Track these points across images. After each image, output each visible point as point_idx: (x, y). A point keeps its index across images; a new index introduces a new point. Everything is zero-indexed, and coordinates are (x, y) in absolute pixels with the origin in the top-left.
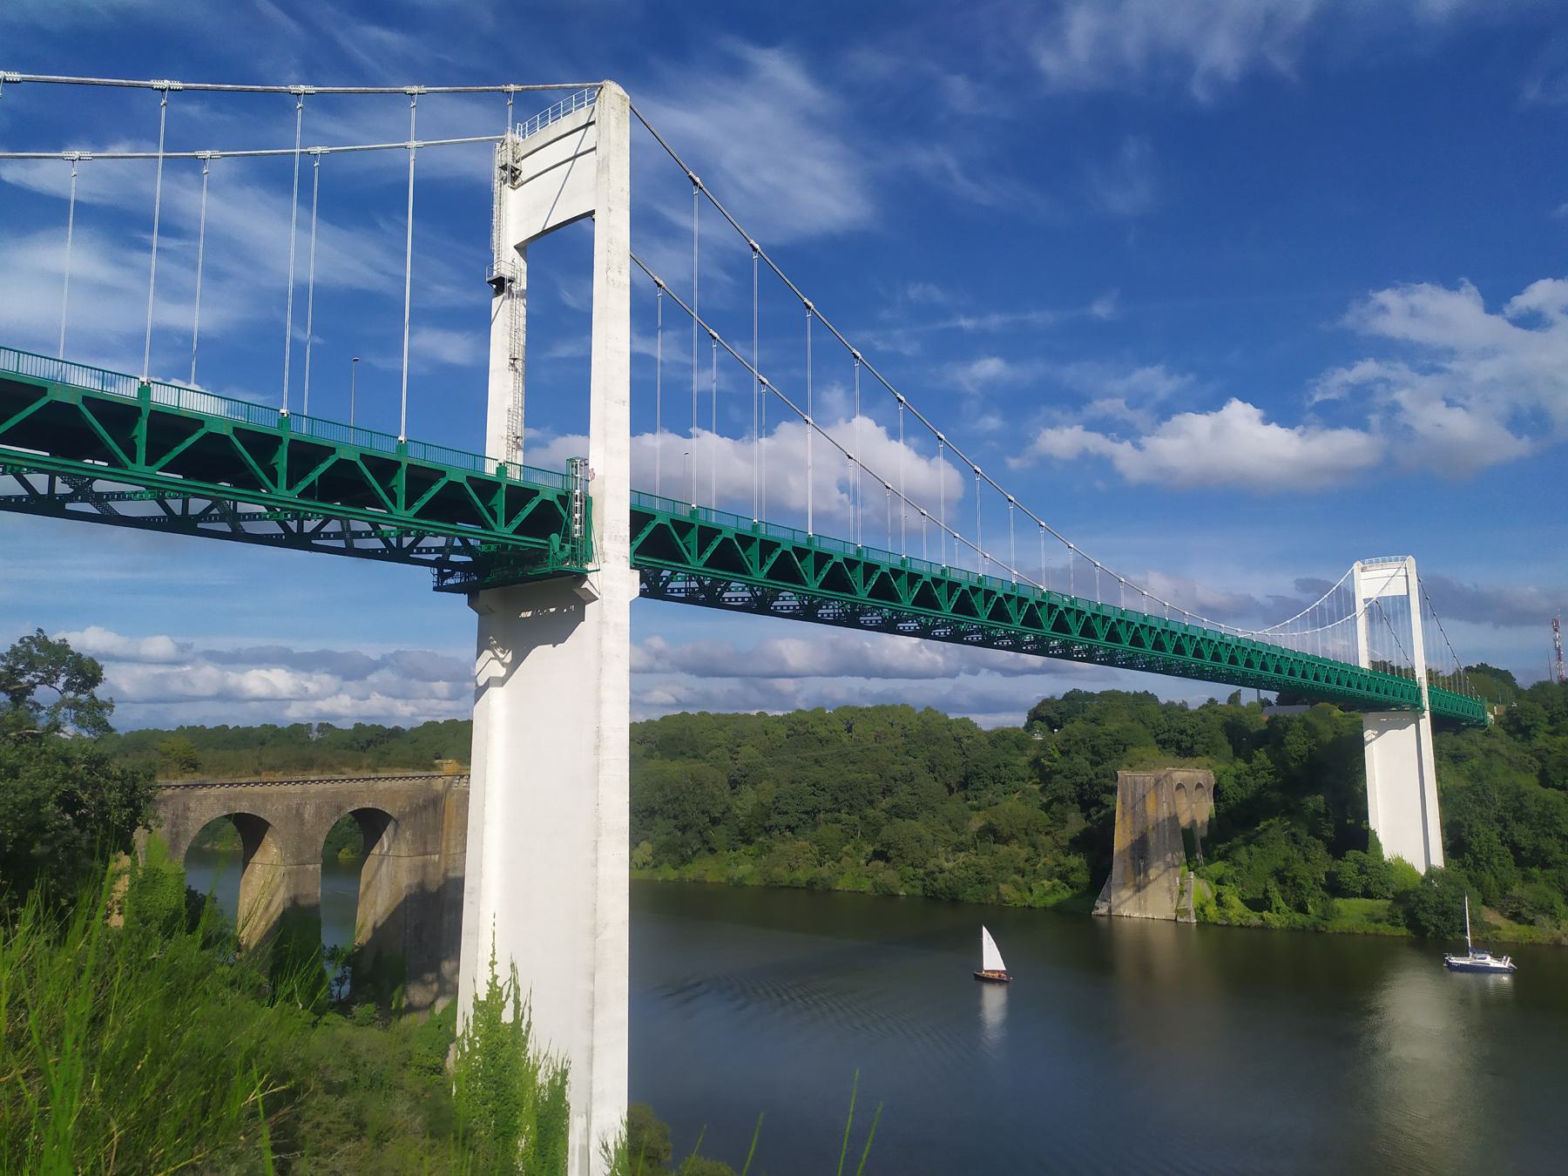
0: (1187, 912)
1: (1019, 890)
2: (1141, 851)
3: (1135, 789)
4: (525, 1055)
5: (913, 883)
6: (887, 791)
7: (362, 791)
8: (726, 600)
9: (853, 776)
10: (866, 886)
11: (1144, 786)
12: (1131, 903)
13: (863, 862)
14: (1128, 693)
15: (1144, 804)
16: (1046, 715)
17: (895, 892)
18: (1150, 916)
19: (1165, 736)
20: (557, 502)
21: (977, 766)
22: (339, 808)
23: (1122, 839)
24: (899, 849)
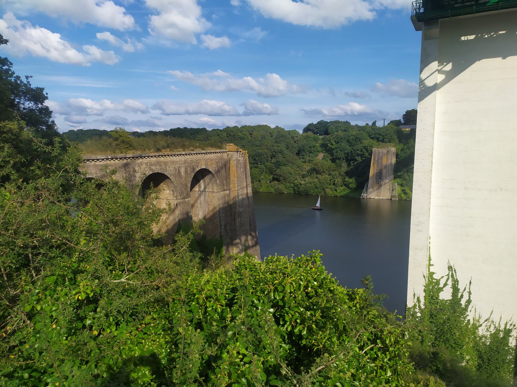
0: (395, 196)
1: (332, 190)
2: (379, 176)
3: (379, 154)
4: (465, 318)
5: (289, 189)
6: (273, 156)
7: (200, 160)
9: (260, 151)
10: (272, 190)
11: (383, 153)
12: (373, 194)
13: (268, 182)
14: (342, 122)
15: (382, 160)
17: (283, 192)
19: (373, 136)
21: (303, 147)
22: (194, 169)
23: (372, 171)
24: (284, 177)
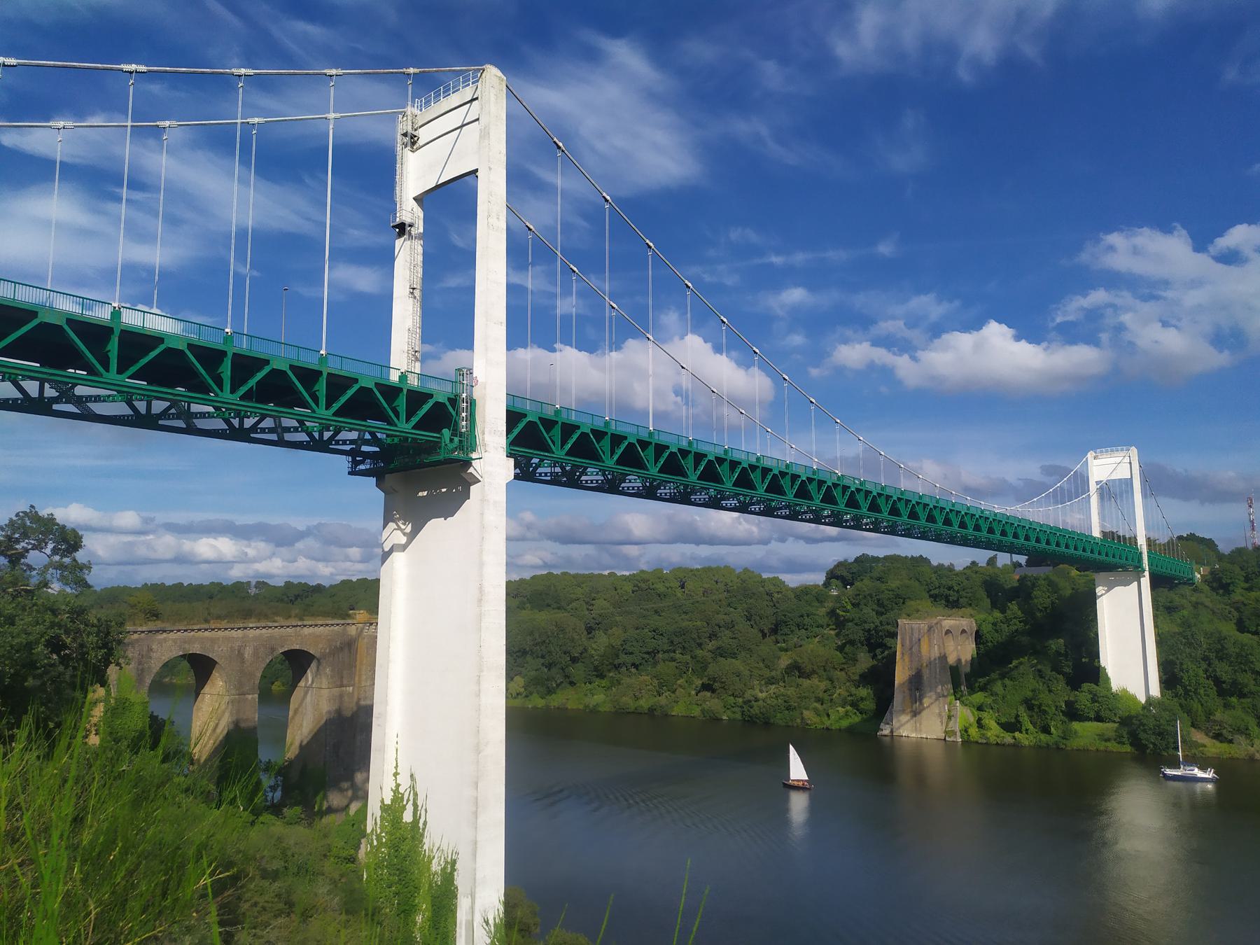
0: (954, 733)
1: (819, 715)
2: (917, 684)
3: (912, 634)
4: (422, 848)
5: (733, 709)
6: (713, 636)
7: (291, 636)
8: (584, 482)
9: (685, 624)
10: (696, 712)
11: (919, 631)
12: (908, 726)
13: (693, 692)
14: (906, 557)
15: (919, 646)
16: (841, 575)
17: (719, 717)
18: (924, 736)
19: (936, 592)
20: (447, 404)
21: (785, 616)
22: (273, 650)
23: (901, 674)
24: (723, 683)
